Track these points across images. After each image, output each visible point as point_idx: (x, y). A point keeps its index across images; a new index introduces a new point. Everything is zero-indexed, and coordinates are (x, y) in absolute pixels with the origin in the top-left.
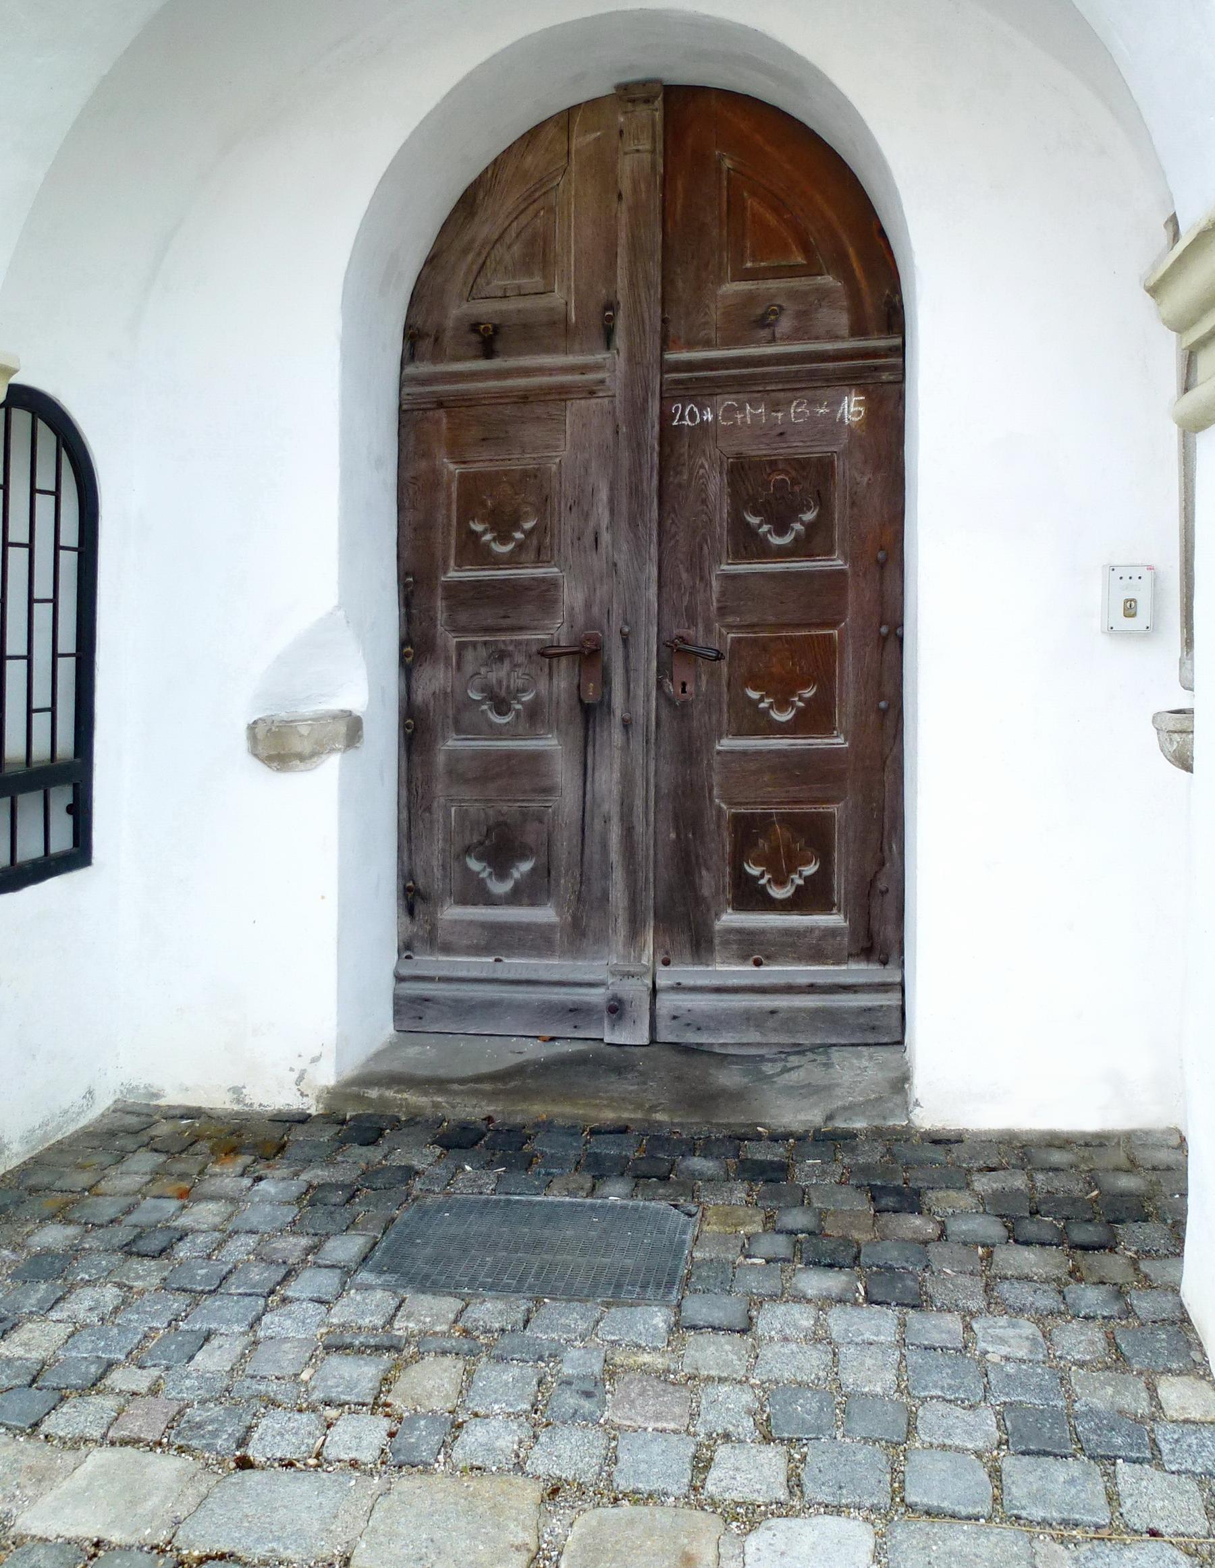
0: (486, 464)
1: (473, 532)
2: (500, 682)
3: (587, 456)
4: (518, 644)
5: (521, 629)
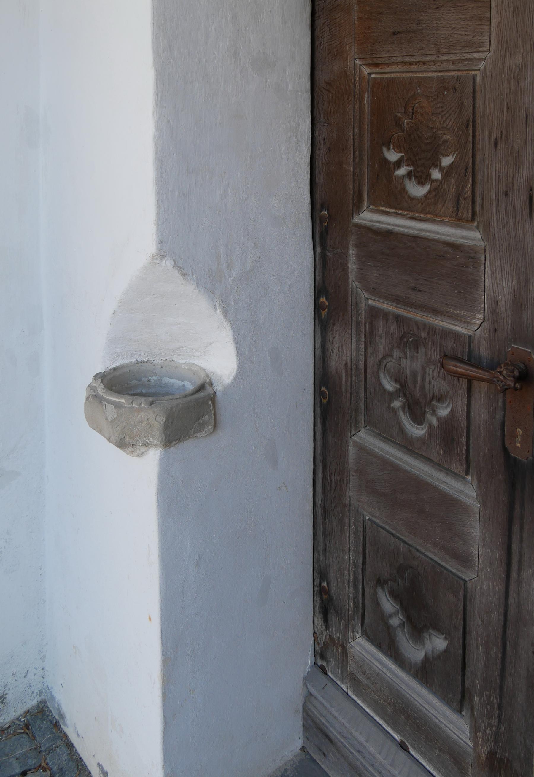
0: (400, 68)
1: (386, 161)
2: (414, 374)
3: (519, 60)
4: (432, 330)
5: (436, 312)
